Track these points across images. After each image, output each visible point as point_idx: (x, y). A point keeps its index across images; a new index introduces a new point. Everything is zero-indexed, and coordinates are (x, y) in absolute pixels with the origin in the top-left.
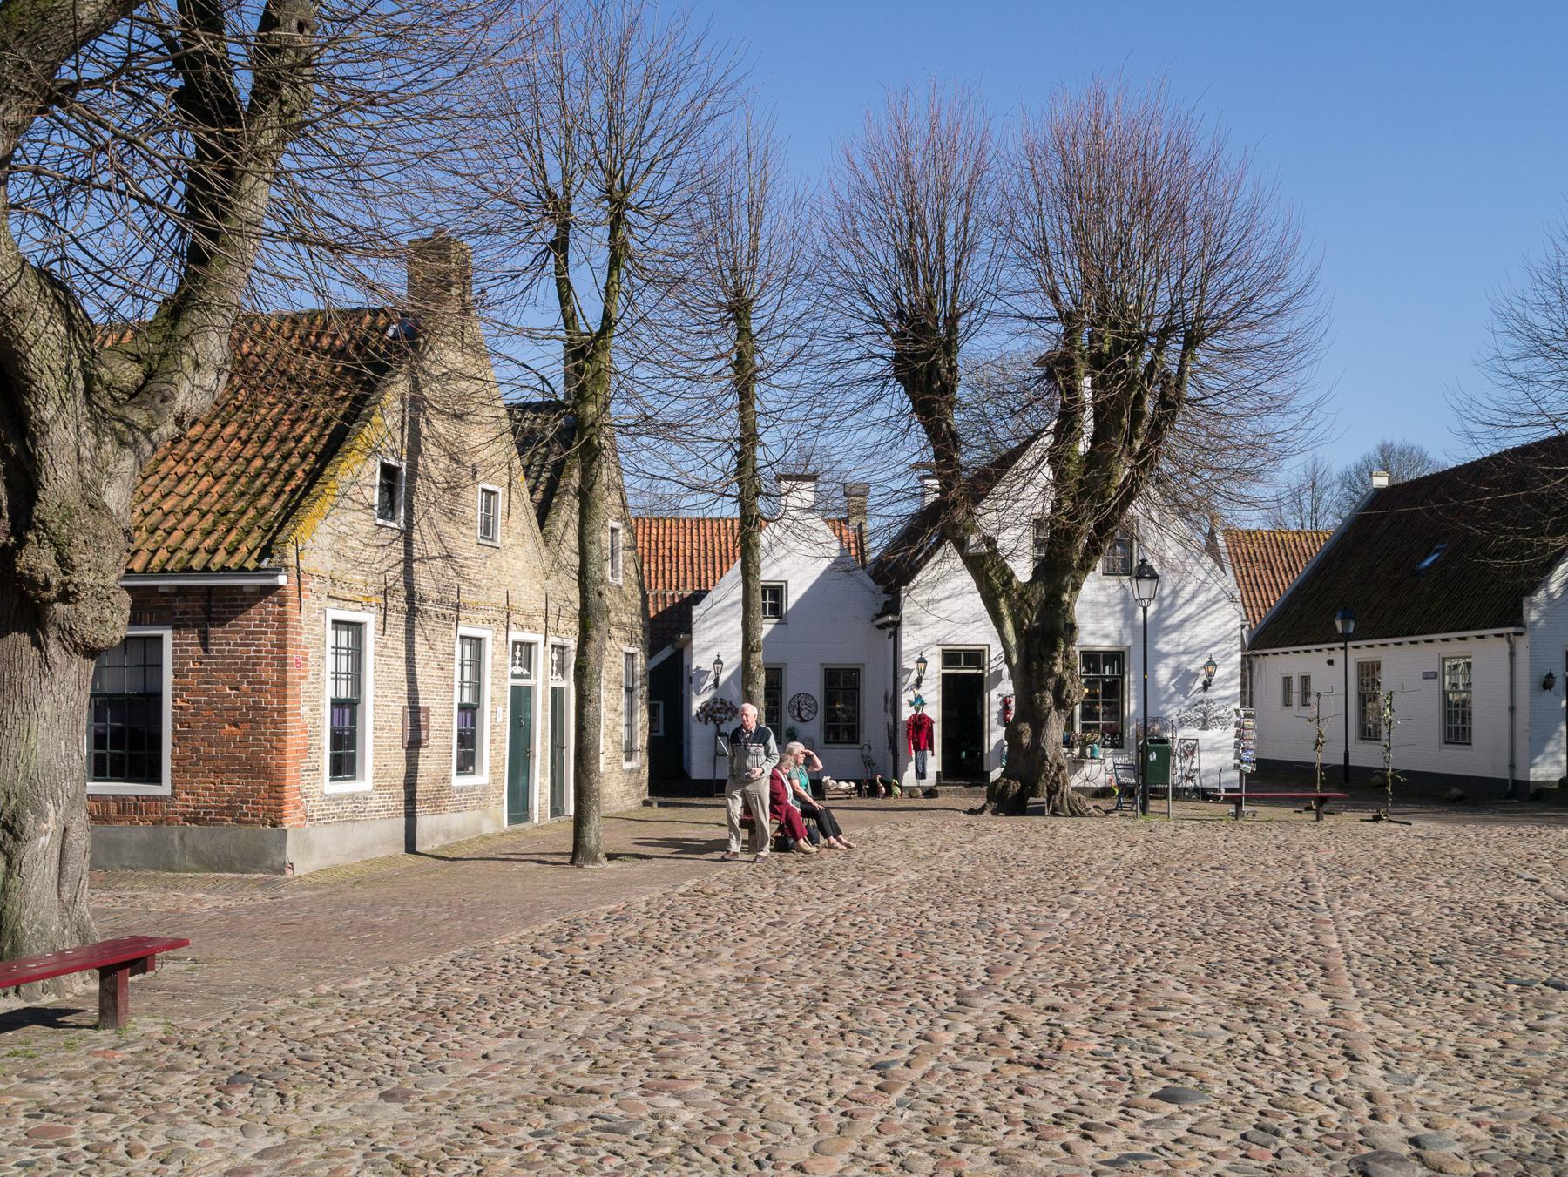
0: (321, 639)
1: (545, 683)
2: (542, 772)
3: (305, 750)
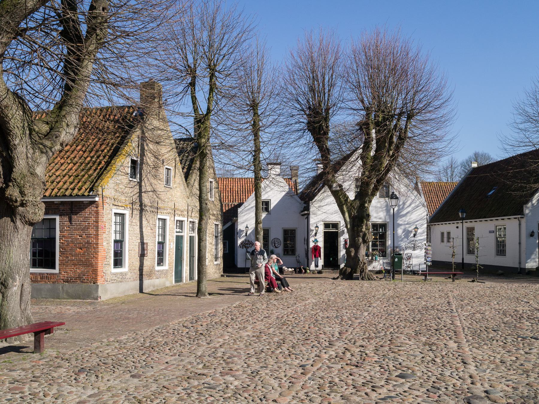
0: (110, 219)
1: (187, 234)
2: (186, 265)
3: (105, 258)
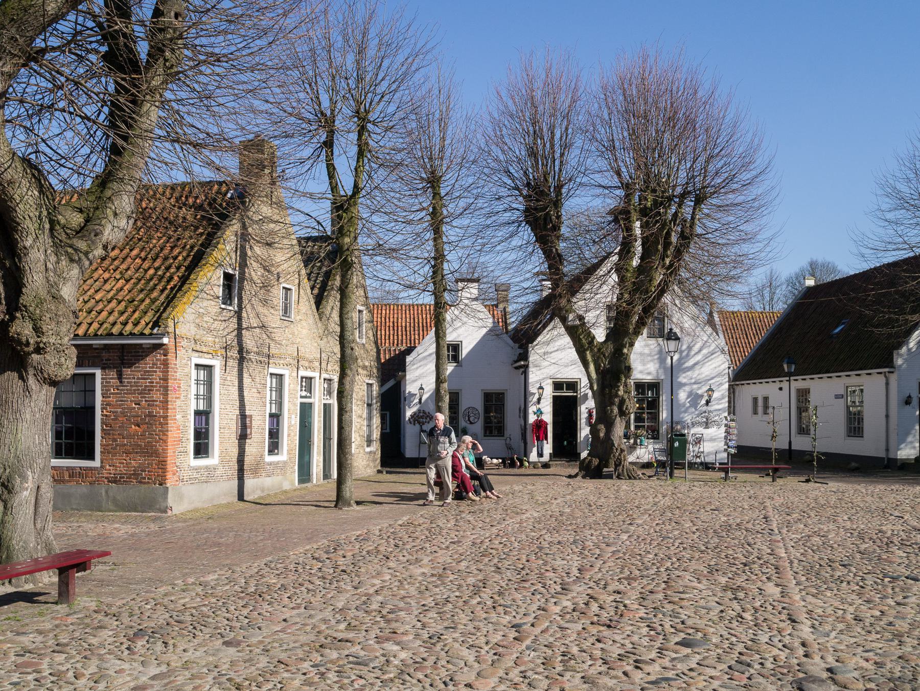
0: (188, 375)
1: (320, 401)
2: (318, 453)
3: (179, 441)
